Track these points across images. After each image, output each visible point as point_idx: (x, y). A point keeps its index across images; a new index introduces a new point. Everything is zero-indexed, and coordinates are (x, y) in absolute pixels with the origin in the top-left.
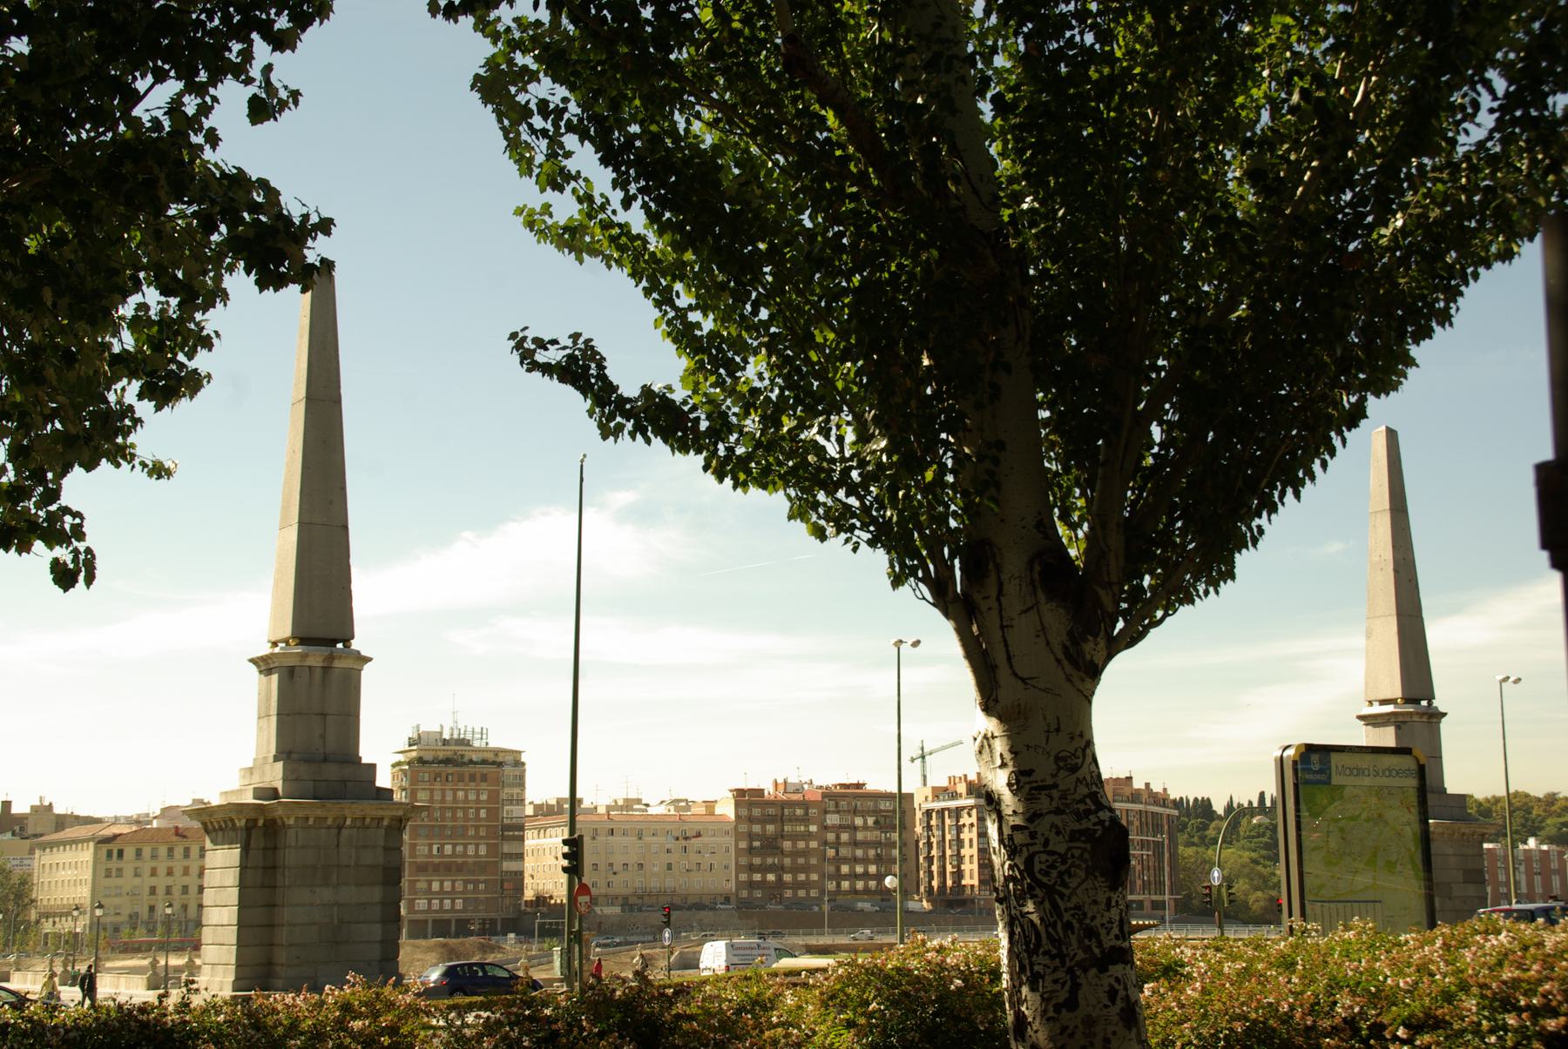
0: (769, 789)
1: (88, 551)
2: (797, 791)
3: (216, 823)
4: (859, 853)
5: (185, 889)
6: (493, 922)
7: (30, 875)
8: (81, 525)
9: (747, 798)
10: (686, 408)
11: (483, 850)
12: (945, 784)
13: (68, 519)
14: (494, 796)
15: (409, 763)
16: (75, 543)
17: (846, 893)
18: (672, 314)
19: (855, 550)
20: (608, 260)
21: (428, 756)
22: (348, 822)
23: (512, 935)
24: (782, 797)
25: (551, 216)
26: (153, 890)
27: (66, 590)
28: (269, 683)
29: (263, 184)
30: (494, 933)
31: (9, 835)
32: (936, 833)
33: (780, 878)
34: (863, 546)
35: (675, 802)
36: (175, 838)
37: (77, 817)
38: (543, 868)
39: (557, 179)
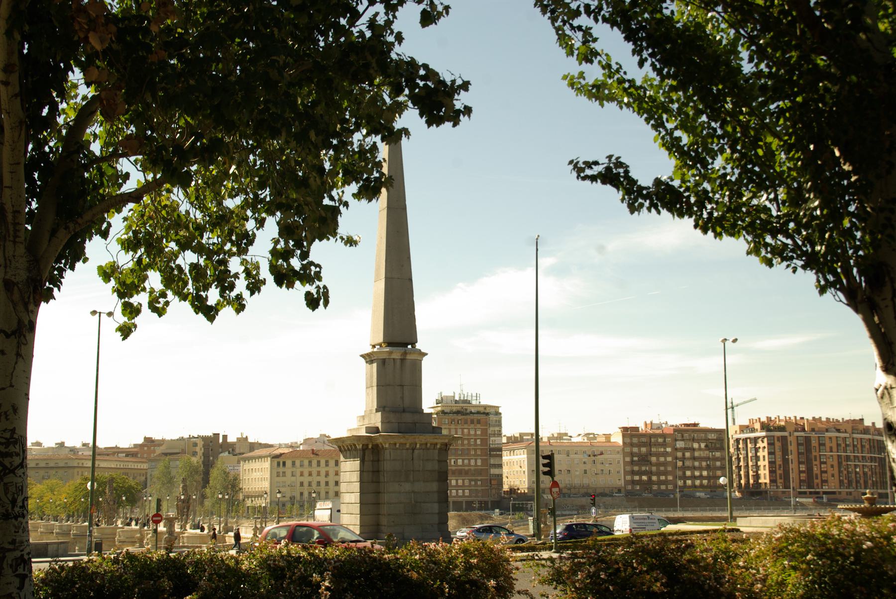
0: (642, 427)
1: (325, 287)
2: (658, 428)
3: (347, 447)
4: (697, 464)
5: (319, 483)
6: (486, 503)
7: (239, 475)
8: (320, 272)
9: (629, 432)
10: (682, 190)
11: (479, 462)
12: (747, 423)
13: (313, 268)
14: (485, 432)
15: (437, 414)
16: (317, 283)
17: (690, 487)
18: (663, 133)
19: (794, 272)
20: (620, 103)
21: (447, 410)
22: (418, 446)
23: (497, 510)
24: (650, 431)
25: (584, 79)
26: (302, 484)
27: (313, 310)
28: (372, 368)
29: (425, 66)
30: (487, 509)
31: (227, 453)
32: (743, 452)
33: (650, 479)
34: (800, 270)
35: (587, 435)
36: (312, 456)
37: (260, 444)
38: (516, 470)
39: (588, 56)
